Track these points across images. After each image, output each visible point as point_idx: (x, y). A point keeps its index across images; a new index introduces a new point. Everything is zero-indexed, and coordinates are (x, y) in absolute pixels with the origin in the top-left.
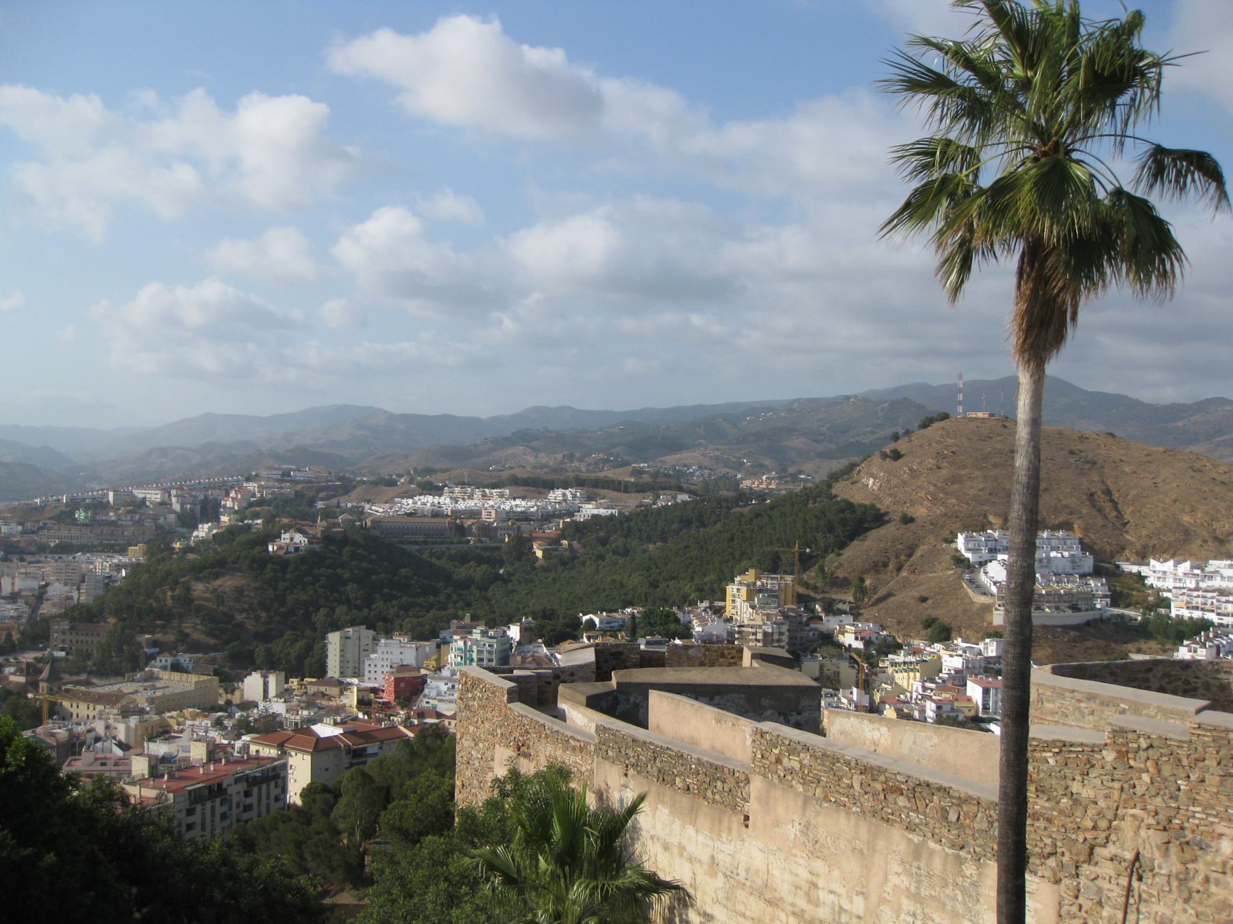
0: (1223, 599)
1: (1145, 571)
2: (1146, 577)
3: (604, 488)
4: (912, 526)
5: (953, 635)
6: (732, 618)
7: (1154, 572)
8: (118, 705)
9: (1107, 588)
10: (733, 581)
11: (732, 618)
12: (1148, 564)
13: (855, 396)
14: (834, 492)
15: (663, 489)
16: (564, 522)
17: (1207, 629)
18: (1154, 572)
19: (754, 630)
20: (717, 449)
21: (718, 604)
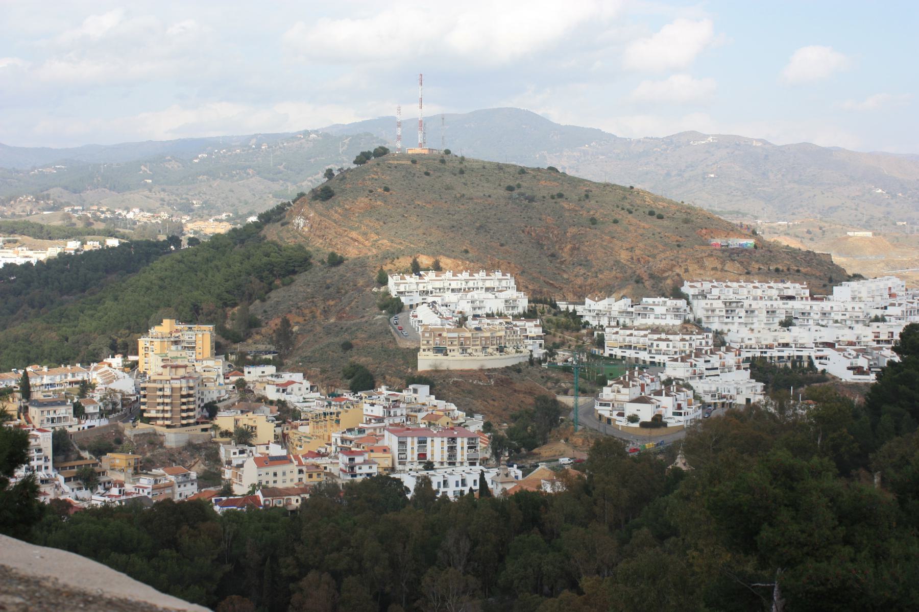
0: (656, 336)
1: (580, 310)
2: (582, 316)
3: (22, 234)
4: (341, 268)
5: (377, 384)
6: (145, 373)
7: (590, 311)
8: (806, 417)
9: (541, 329)
10: (824, 371)
11: (145, 373)
12: (584, 304)
13: (316, 132)
14: (262, 233)
15: (89, 234)
16: (598, 334)
17: (632, 368)
18: (590, 311)
19: (160, 386)
20: (164, 190)
21: (132, 358)
